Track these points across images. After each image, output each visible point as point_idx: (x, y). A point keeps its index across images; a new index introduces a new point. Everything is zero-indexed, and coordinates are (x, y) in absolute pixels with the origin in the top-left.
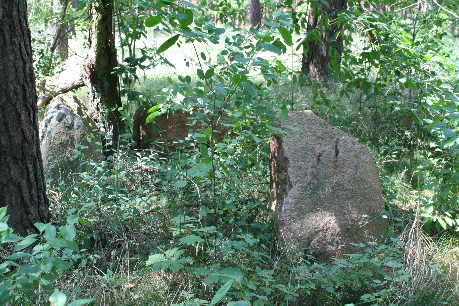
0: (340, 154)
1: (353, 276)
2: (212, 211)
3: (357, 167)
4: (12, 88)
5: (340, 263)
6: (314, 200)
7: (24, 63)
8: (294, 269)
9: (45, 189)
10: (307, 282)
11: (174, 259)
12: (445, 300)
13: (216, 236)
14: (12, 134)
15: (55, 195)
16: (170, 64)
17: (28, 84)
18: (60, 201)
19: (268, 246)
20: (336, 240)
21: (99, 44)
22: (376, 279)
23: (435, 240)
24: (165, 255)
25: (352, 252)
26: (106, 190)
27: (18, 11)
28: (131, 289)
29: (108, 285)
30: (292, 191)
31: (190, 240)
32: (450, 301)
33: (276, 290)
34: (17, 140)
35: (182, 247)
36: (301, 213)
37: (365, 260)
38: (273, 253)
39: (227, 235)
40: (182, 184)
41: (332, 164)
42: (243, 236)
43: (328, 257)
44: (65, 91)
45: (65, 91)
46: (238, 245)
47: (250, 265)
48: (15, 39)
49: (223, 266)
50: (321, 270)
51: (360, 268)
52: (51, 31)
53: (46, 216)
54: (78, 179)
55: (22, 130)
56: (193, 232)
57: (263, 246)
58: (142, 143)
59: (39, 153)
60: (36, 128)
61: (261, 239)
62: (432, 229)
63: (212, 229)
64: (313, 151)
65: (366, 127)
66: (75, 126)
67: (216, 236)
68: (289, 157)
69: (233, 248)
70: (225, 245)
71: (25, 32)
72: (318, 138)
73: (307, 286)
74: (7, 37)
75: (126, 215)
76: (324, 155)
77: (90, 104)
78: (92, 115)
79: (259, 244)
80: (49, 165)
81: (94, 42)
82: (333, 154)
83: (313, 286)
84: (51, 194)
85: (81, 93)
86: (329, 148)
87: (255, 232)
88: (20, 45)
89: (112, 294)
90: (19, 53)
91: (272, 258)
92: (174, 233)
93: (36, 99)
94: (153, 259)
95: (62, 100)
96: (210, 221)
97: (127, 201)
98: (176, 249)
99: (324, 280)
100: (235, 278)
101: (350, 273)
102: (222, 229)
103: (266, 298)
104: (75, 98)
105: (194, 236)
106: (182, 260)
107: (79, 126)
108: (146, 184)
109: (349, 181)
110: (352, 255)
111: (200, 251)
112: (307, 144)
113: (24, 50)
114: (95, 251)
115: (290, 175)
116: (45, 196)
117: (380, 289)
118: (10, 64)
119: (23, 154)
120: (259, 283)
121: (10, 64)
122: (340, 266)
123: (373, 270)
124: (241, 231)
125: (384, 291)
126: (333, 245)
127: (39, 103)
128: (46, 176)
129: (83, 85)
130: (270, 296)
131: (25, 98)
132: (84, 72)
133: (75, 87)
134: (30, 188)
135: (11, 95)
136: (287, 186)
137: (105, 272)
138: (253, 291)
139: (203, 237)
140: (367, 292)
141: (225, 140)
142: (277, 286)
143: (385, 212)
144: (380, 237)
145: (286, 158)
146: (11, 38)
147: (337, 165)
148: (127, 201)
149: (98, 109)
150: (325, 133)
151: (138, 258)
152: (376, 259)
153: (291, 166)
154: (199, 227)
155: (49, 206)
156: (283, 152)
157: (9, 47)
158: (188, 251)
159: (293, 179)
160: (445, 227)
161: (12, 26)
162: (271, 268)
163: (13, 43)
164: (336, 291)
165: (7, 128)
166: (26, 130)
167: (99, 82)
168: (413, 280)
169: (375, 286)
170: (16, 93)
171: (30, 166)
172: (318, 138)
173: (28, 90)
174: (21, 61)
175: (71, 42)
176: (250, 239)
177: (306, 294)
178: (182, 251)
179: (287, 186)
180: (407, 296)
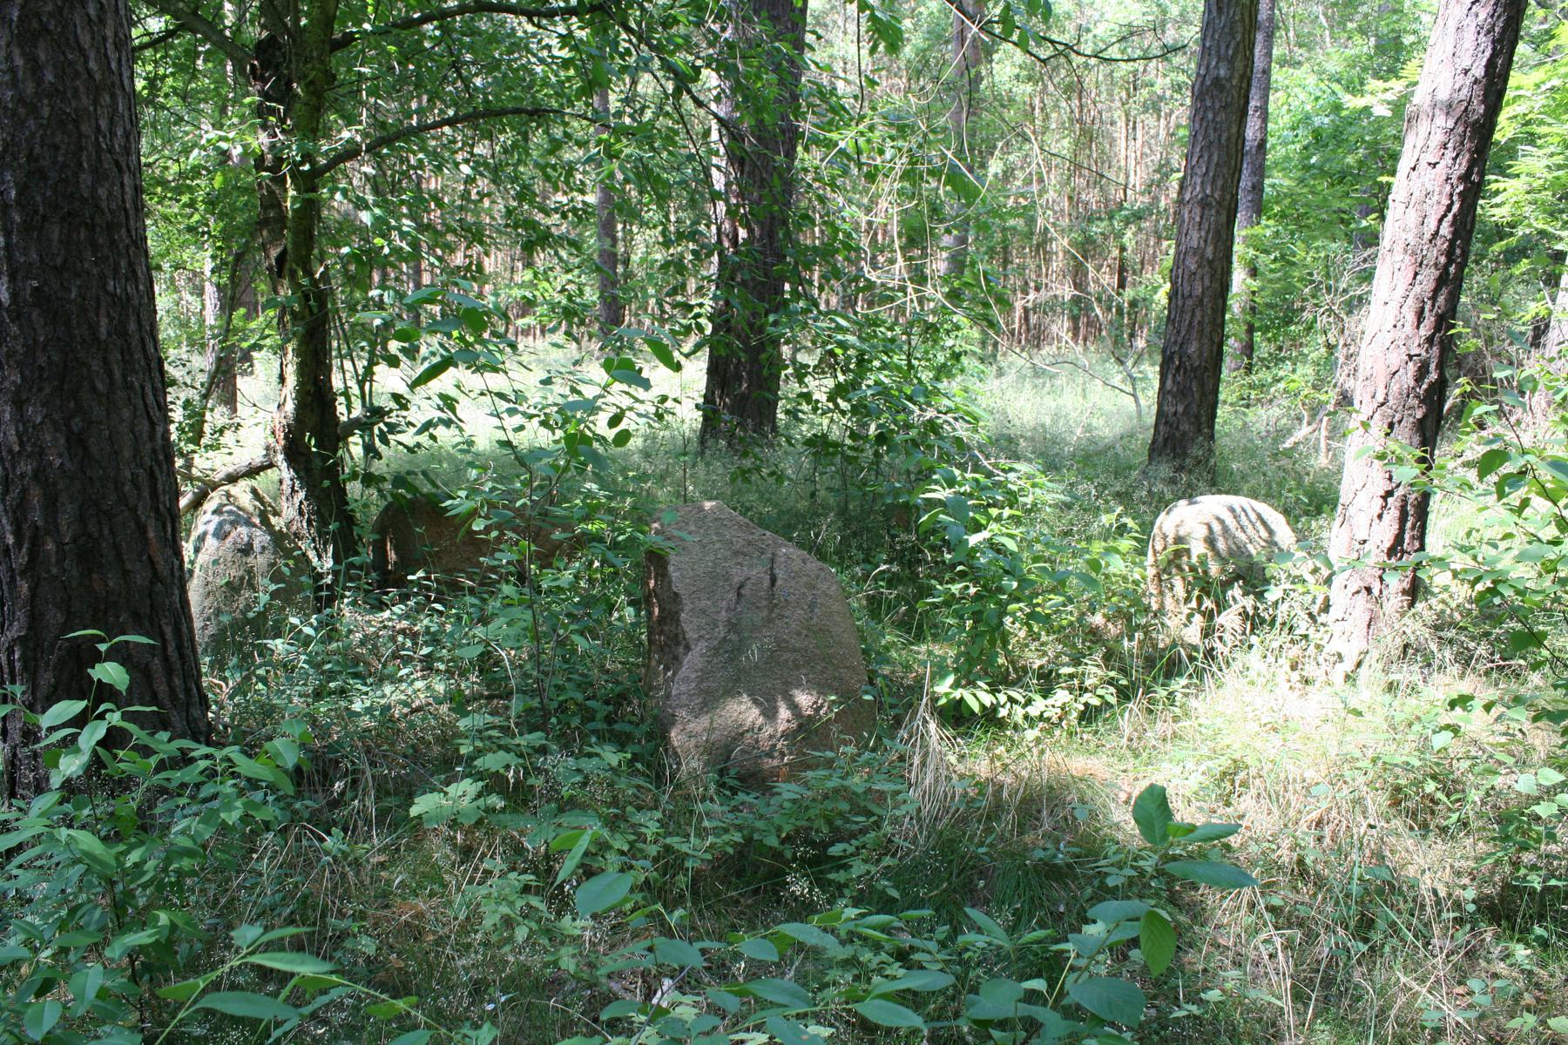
0: (779, 582)
1: (812, 813)
2: (535, 703)
3: (812, 606)
4: (128, 474)
5: (788, 790)
6: (731, 674)
7: (152, 424)
8: (700, 807)
9: (200, 675)
10: (726, 831)
11: (466, 802)
12: (981, 844)
13: (543, 750)
14: (129, 566)
15: (220, 687)
16: (465, 414)
17: (160, 466)
18: (231, 698)
19: (649, 766)
20: (779, 746)
21: (301, 384)
22: (857, 814)
23: (963, 735)
24: (446, 793)
25: (809, 767)
26: (323, 673)
27: (139, 322)
28: (382, 865)
29: (335, 858)
30: (689, 657)
31: (492, 762)
32: (991, 845)
33: (668, 849)
34: (141, 578)
35: (479, 776)
36: (709, 700)
37: (834, 782)
38: (659, 780)
39: (566, 745)
40: (474, 652)
41: (764, 603)
42: (597, 750)
43: (764, 780)
44: (232, 479)
45: (232, 479)
46: (588, 765)
47: (615, 802)
48: (132, 378)
49: (561, 810)
50: (751, 806)
51: (826, 797)
52: (203, 362)
53: (204, 729)
54: (264, 651)
55: (150, 558)
56: (500, 747)
57: (639, 766)
58: (391, 577)
59: (185, 603)
60: (178, 553)
61: (634, 754)
62: (956, 717)
63: (536, 738)
64: (727, 577)
65: (828, 531)
66: (257, 546)
67: (543, 750)
68: (681, 592)
69: (579, 771)
70: (560, 764)
71: (154, 365)
72: (736, 553)
73: (726, 837)
74: (118, 375)
75: (366, 722)
76: (749, 586)
77: (285, 505)
78: (289, 525)
79: (631, 763)
80: (205, 628)
81: (291, 380)
82: (766, 583)
83: (737, 837)
84: (211, 686)
85: (264, 481)
86: (758, 572)
87: (622, 741)
88: (143, 388)
89: (344, 876)
90: (141, 406)
91: (658, 788)
92: (463, 751)
93: (177, 494)
94: (422, 805)
95: (228, 495)
96: (531, 722)
97: (366, 693)
98: (468, 781)
99: (760, 824)
100: (592, 829)
101: (807, 808)
102: (557, 739)
103: (647, 863)
104: (254, 491)
105: (501, 753)
106: (481, 802)
107: (264, 548)
108: (402, 657)
109: (799, 634)
110: (809, 774)
111: (517, 782)
112: (715, 565)
113: (150, 399)
114: (306, 794)
115: (686, 628)
116: (199, 687)
117: (863, 831)
118: (124, 428)
119: (152, 606)
120: (633, 837)
121: (124, 428)
122: (786, 796)
123: (851, 801)
124: (594, 739)
125: (873, 834)
126: (773, 758)
127: (183, 502)
128: (200, 650)
129: (271, 466)
130: (656, 860)
131: (154, 495)
132: (271, 440)
133: (253, 472)
134: (169, 671)
135: (127, 488)
136: (681, 649)
137: (329, 834)
138: (622, 853)
139: (521, 756)
140: (840, 841)
141: (556, 563)
142: (668, 841)
143: (869, 688)
144: (861, 735)
145: (676, 594)
146: (124, 376)
147: (773, 601)
148: (366, 693)
149: (301, 513)
150: (749, 543)
151: (391, 802)
152: (856, 779)
153: (687, 608)
154: (513, 736)
155: (208, 708)
156: (670, 582)
157: (121, 394)
158: (494, 782)
159: (691, 635)
160: (976, 708)
161: (126, 352)
162: (656, 808)
163: (128, 387)
164: (783, 842)
165: (119, 555)
166: (158, 558)
167: (302, 459)
168: (924, 813)
169: (854, 827)
170: (136, 486)
171: (168, 630)
172: (736, 553)
173: (161, 478)
174: (146, 422)
175: (241, 382)
176: (611, 756)
177: (726, 853)
178: (480, 784)
179: (681, 649)
180: (914, 841)
